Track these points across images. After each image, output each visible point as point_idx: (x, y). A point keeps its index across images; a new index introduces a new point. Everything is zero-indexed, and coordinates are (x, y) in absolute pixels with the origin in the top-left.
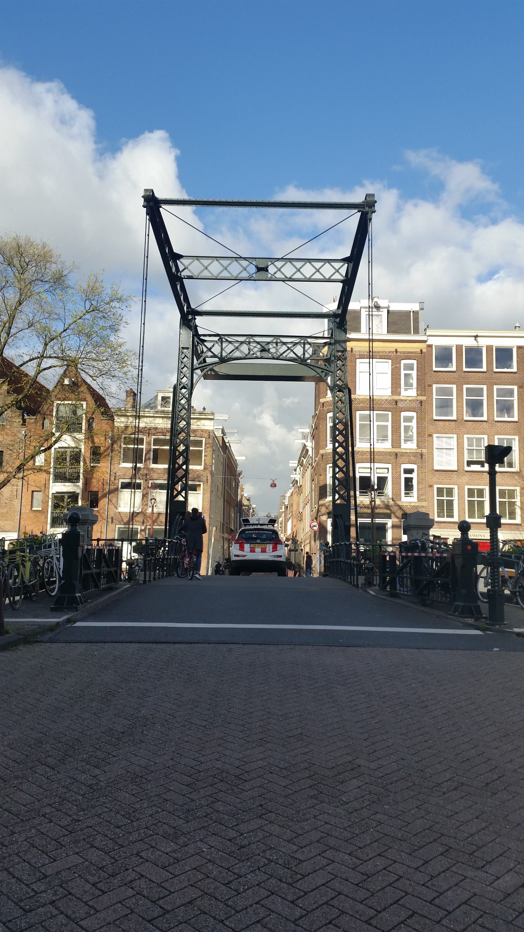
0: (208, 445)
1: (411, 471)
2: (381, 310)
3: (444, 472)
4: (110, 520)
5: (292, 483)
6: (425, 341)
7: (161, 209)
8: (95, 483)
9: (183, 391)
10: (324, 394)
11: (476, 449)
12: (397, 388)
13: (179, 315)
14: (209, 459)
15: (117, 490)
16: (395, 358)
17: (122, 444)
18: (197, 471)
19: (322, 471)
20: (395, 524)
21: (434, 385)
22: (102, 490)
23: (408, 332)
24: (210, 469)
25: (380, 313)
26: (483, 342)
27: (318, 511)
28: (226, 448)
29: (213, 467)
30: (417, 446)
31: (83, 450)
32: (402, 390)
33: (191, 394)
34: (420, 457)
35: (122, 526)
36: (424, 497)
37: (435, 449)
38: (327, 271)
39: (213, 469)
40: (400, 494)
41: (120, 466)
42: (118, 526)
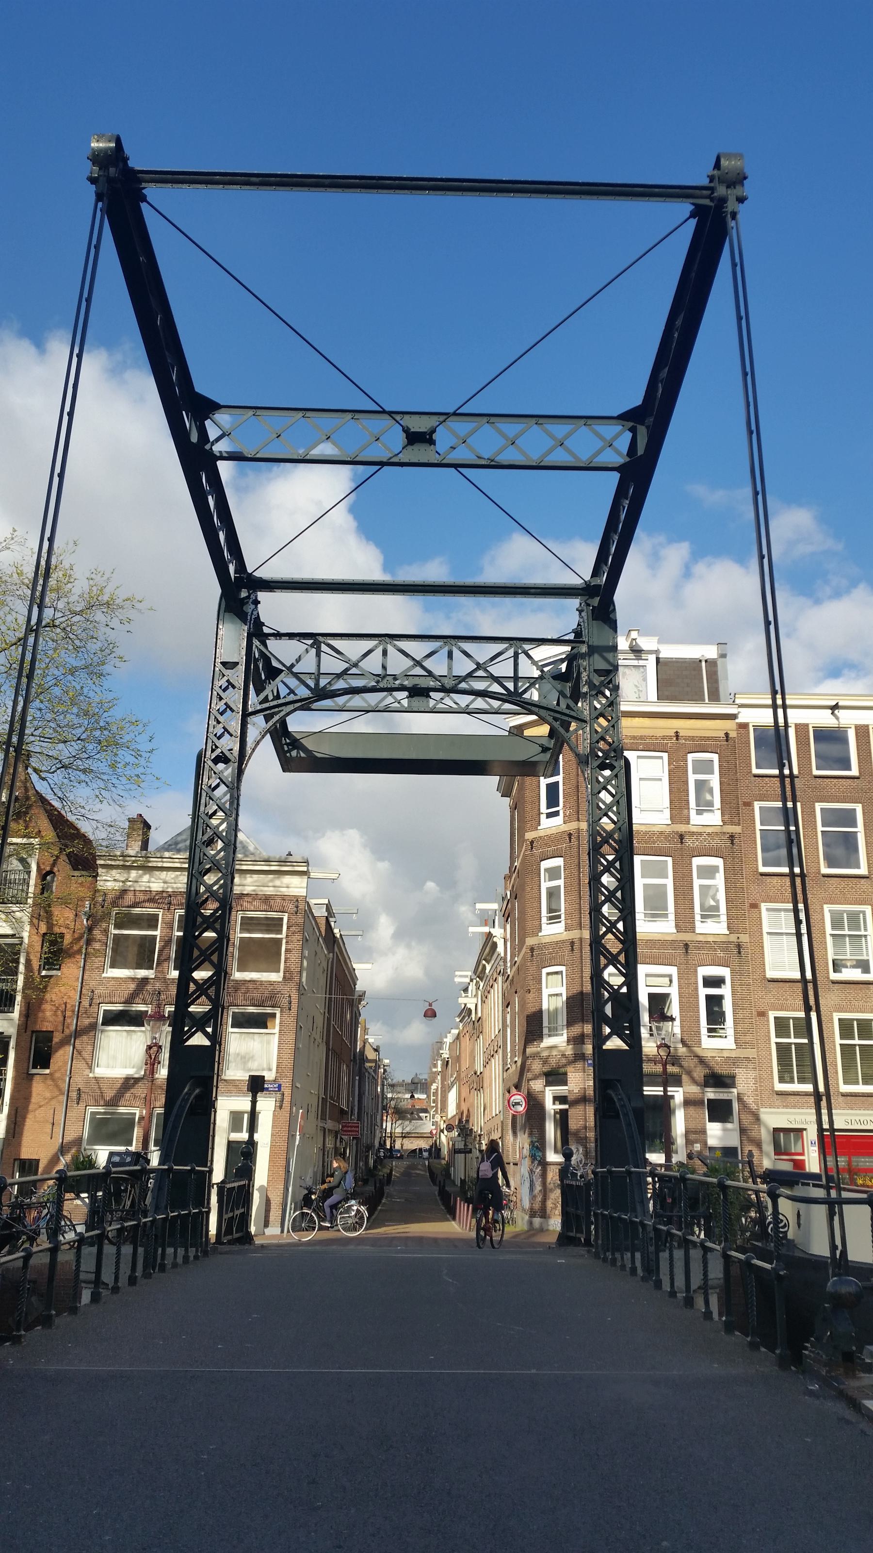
0: (293, 929)
1: (717, 982)
2: (644, 656)
3: (788, 984)
4: (73, 1095)
5: (459, 1016)
6: (733, 717)
7: (144, 206)
8: (48, 1014)
9: (218, 771)
10: (534, 823)
11: (850, 936)
12: (681, 808)
13: (216, 590)
14: (295, 957)
15: (93, 1027)
16: (676, 749)
17: (112, 927)
18: (271, 983)
19: (531, 982)
20: (692, 1097)
21: (756, 803)
22: (60, 1028)
23: (698, 698)
24: (297, 979)
25: (641, 663)
26: (848, 719)
27: (523, 1069)
28: (334, 942)
29: (304, 975)
30: (729, 928)
31: (26, 940)
32: (693, 813)
33: (240, 772)
34: (736, 951)
35: (101, 1109)
36: (748, 1038)
37: (765, 936)
38: (584, 444)
39: (304, 979)
40: (699, 1033)
41: (104, 975)
42: (91, 1109)
